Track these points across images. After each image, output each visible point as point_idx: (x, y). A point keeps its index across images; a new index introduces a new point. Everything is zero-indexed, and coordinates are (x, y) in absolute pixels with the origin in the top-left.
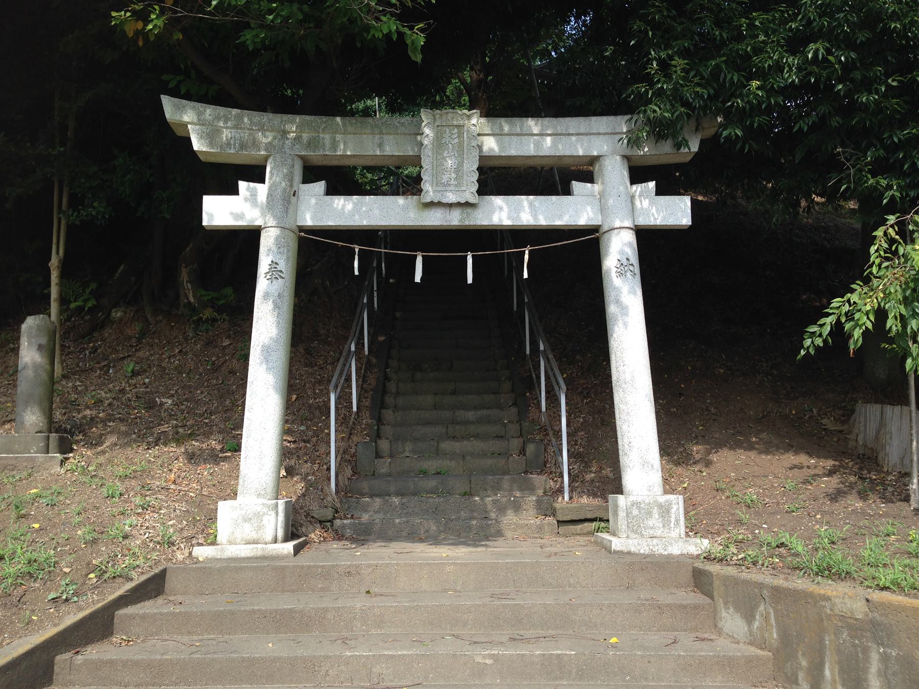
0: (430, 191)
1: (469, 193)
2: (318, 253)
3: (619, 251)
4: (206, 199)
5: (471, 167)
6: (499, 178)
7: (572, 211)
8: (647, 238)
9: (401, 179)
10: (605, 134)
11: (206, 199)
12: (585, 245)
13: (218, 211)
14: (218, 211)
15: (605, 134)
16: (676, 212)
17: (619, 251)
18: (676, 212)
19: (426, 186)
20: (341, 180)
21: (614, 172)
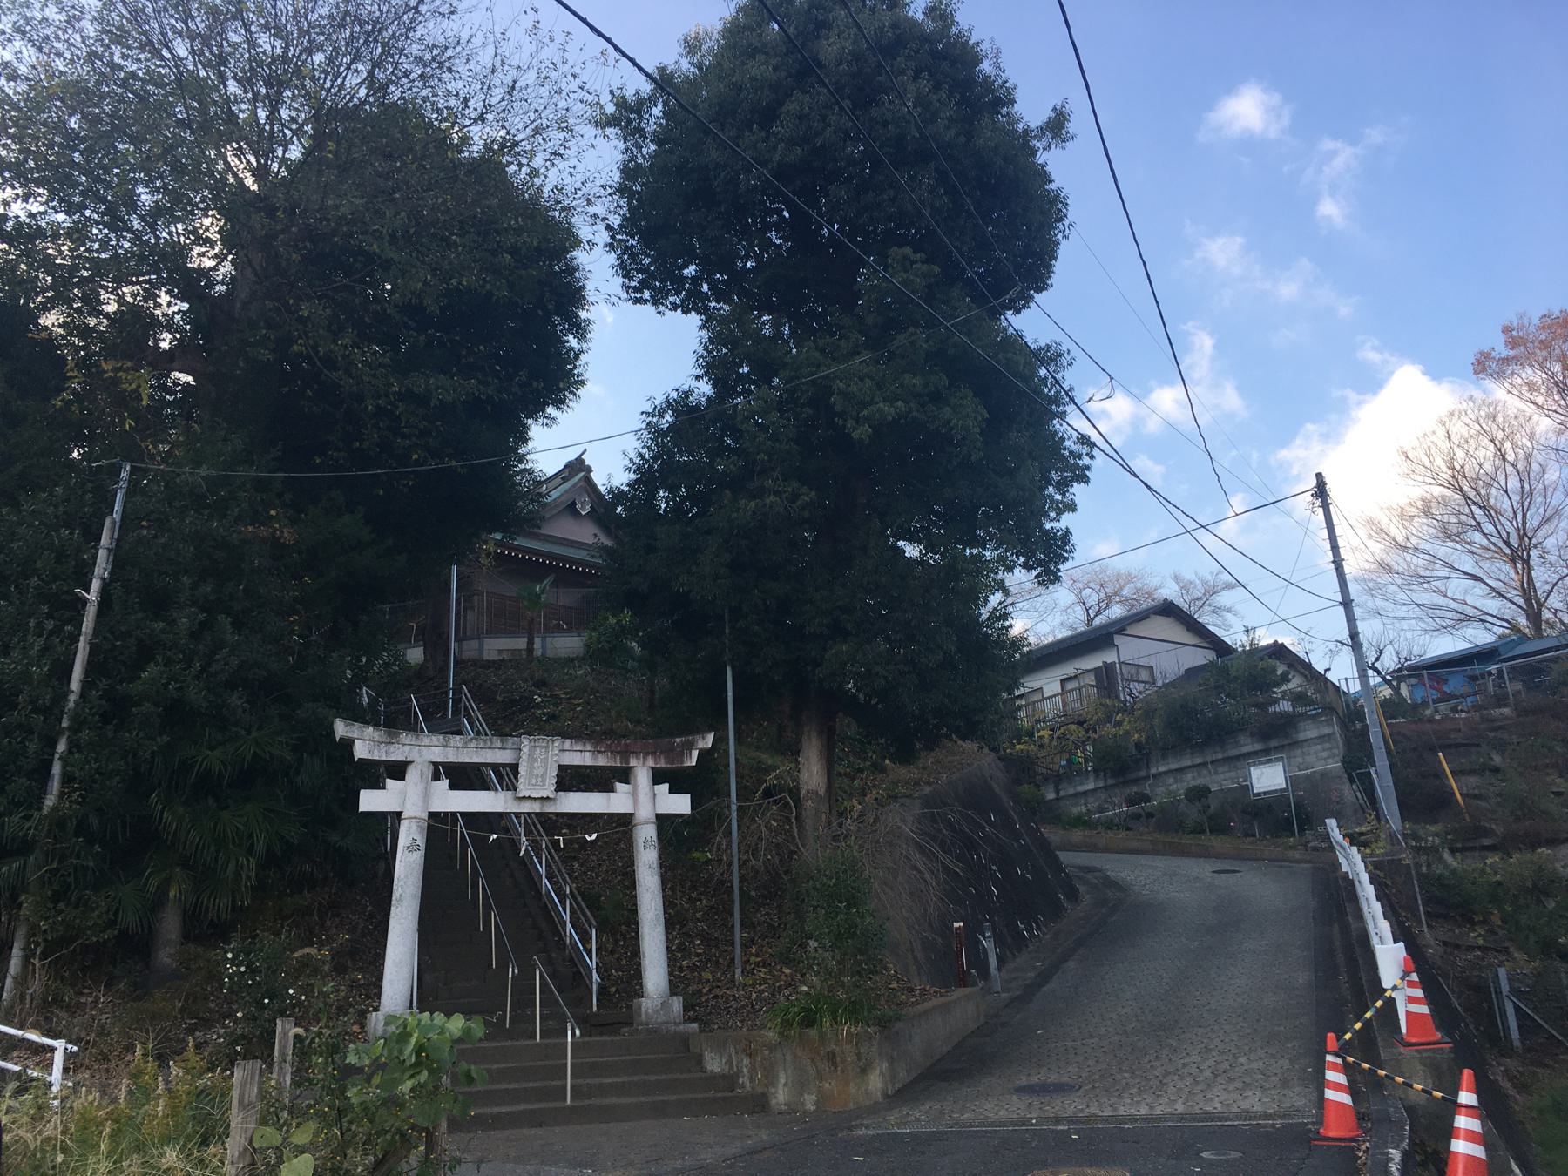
0: (523, 791)
1: (548, 790)
2: (438, 824)
3: (646, 834)
4: (361, 809)
5: (553, 772)
6: (570, 779)
7: (616, 802)
8: (663, 820)
9: (506, 776)
10: (647, 74)
11: (361, 809)
12: (624, 823)
13: (370, 801)
14: (370, 801)
15: (647, 74)
16: (680, 804)
17: (646, 834)
18: (680, 804)
19: (521, 786)
20: (463, 777)
21: (642, 775)
